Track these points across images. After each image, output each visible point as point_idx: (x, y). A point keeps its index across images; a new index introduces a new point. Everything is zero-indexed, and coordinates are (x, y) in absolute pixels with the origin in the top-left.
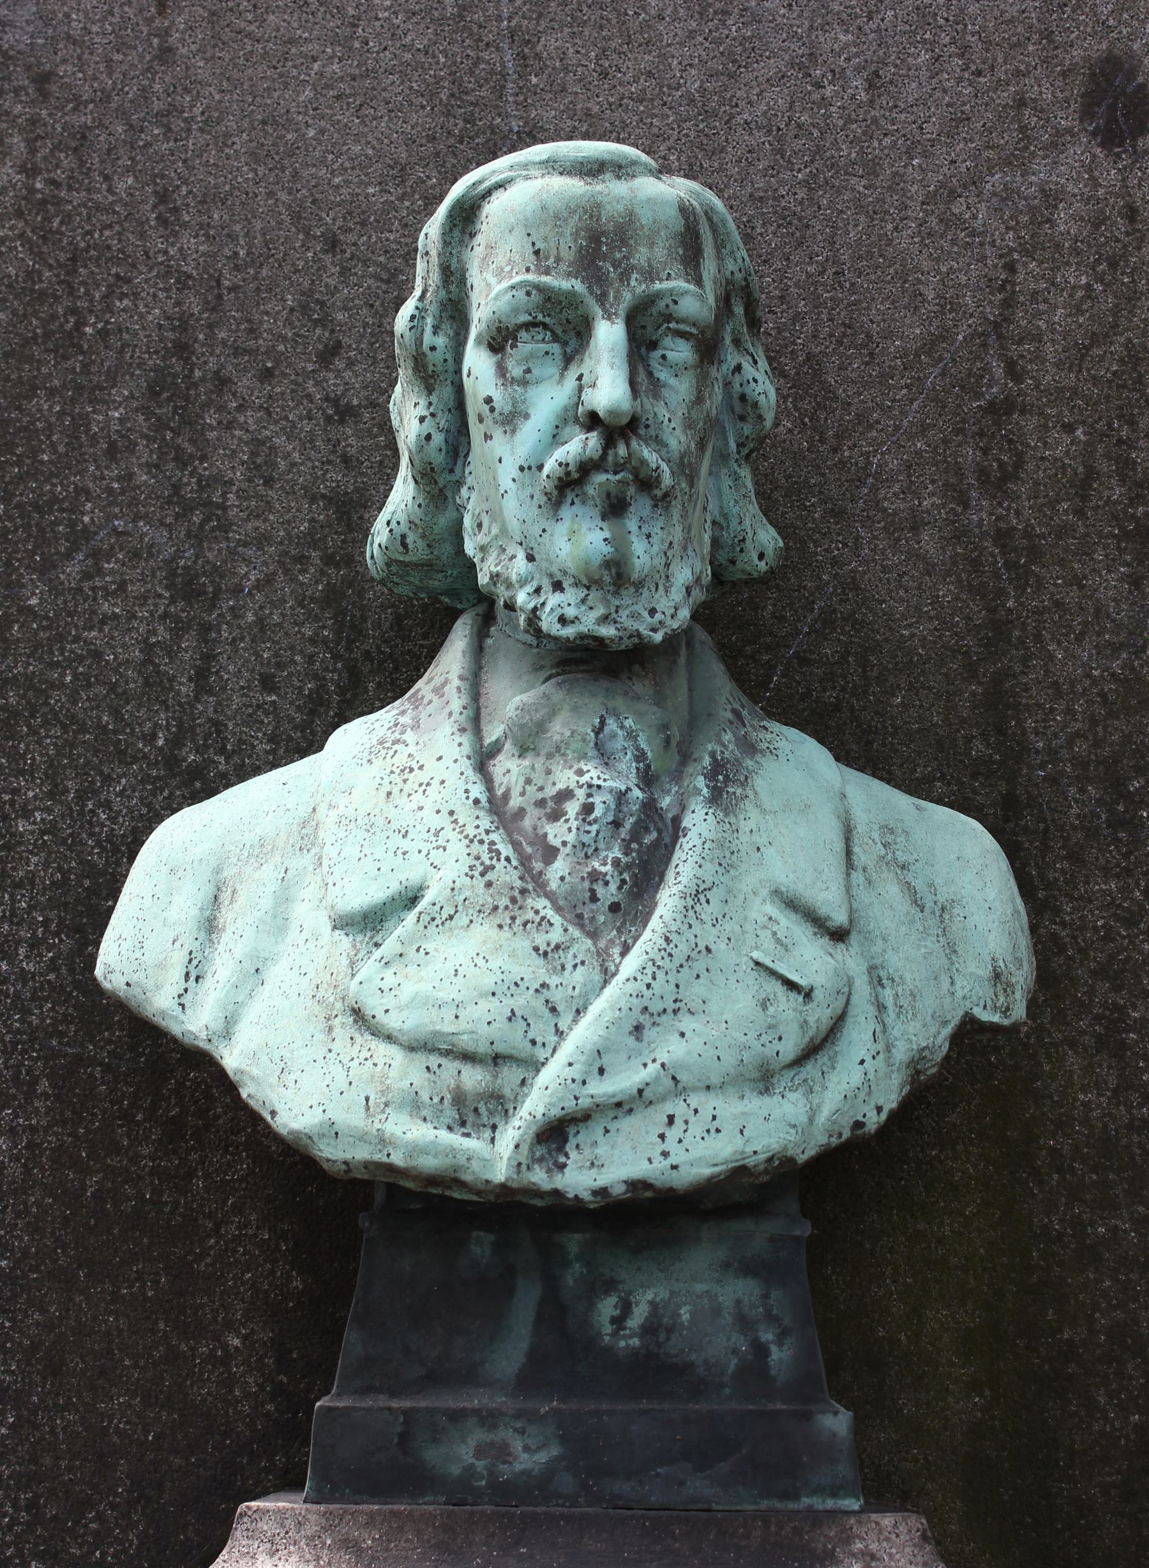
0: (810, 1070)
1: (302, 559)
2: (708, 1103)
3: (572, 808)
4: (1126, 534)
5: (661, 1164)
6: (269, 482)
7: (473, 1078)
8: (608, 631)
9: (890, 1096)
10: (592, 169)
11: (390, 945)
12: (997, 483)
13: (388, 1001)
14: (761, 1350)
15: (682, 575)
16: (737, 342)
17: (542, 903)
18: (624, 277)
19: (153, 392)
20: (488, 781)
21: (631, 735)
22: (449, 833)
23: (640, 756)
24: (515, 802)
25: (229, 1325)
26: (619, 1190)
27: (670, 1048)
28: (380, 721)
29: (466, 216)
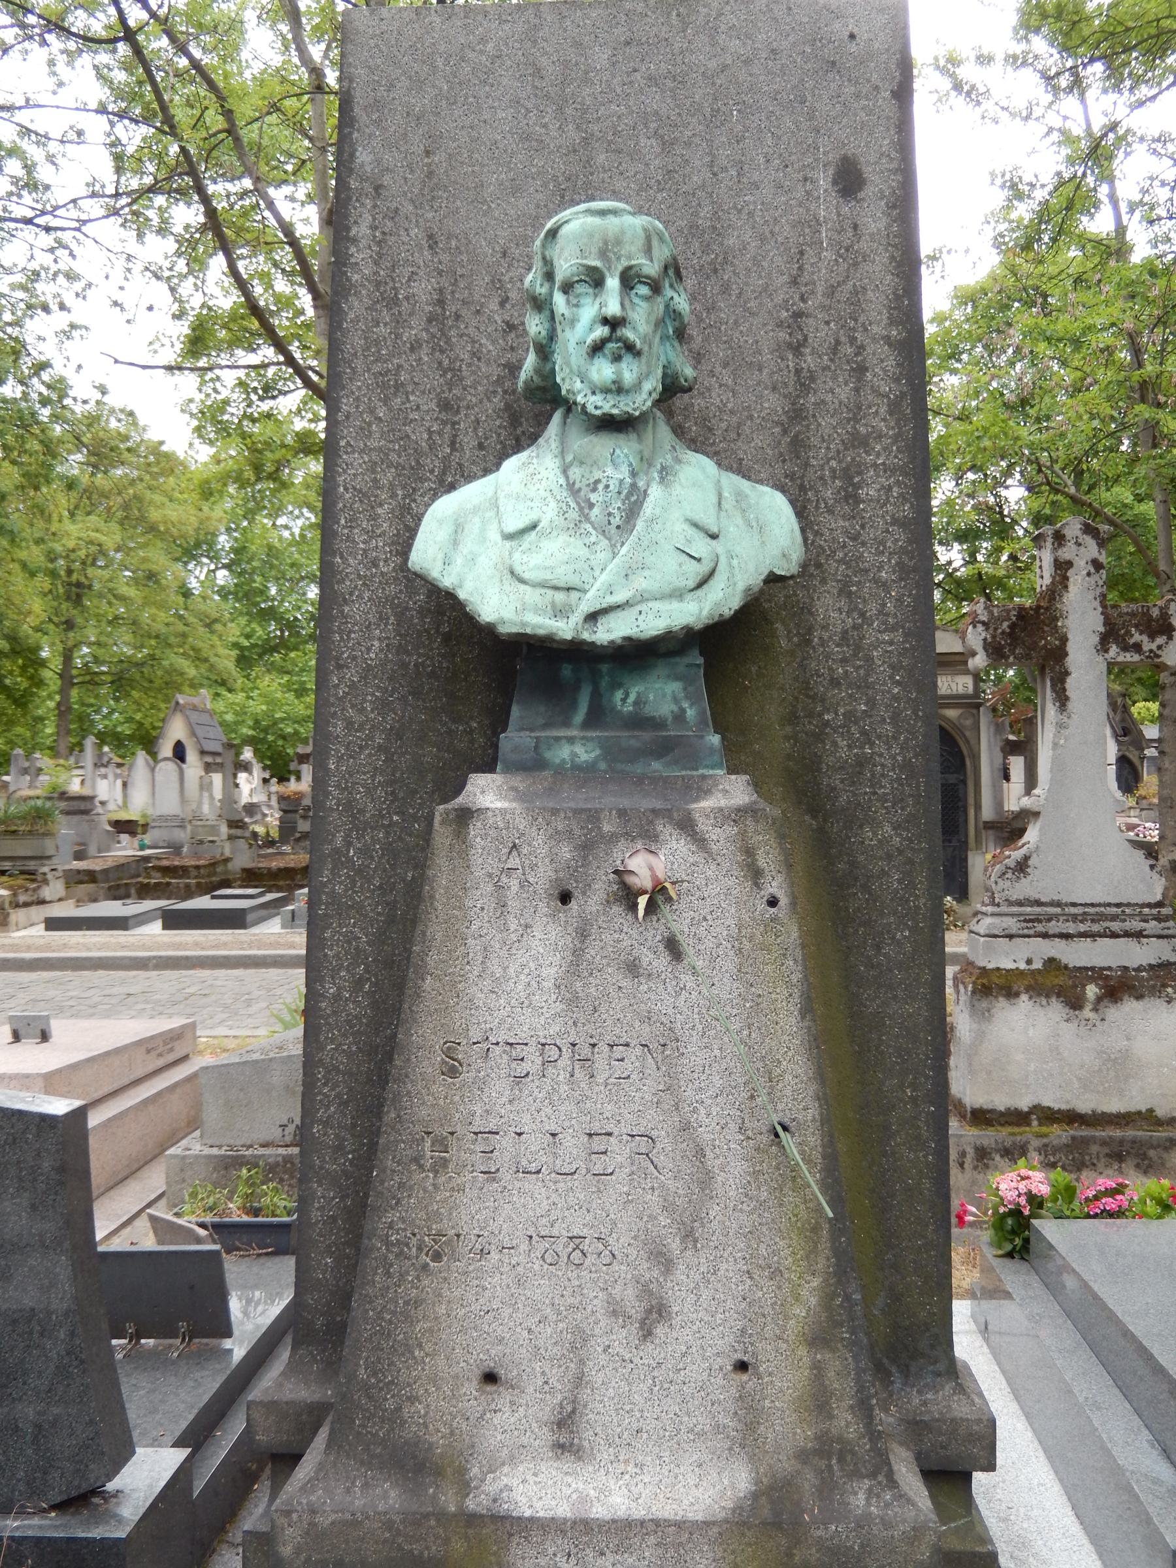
0: (699, 592)
1: (495, 392)
2: (656, 605)
3: (601, 487)
4: (853, 369)
5: (636, 630)
6: (479, 359)
7: (560, 597)
8: (615, 411)
9: (735, 603)
10: (603, 213)
11: (525, 545)
12: (797, 349)
13: (524, 567)
14: (683, 711)
15: (647, 386)
16: (671, 286)
17: (588, 526)
18: (619, 259)
19: (430, 321)
20: (567, 478)
21: (626, 456)
22: (550, 499)
23: (631, 465)
24: (577, 486)
25: (472, 718)
26: (619, 641)
27: (641, 583)
28: (523, 456)
29: (553, 233)
